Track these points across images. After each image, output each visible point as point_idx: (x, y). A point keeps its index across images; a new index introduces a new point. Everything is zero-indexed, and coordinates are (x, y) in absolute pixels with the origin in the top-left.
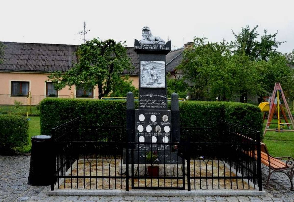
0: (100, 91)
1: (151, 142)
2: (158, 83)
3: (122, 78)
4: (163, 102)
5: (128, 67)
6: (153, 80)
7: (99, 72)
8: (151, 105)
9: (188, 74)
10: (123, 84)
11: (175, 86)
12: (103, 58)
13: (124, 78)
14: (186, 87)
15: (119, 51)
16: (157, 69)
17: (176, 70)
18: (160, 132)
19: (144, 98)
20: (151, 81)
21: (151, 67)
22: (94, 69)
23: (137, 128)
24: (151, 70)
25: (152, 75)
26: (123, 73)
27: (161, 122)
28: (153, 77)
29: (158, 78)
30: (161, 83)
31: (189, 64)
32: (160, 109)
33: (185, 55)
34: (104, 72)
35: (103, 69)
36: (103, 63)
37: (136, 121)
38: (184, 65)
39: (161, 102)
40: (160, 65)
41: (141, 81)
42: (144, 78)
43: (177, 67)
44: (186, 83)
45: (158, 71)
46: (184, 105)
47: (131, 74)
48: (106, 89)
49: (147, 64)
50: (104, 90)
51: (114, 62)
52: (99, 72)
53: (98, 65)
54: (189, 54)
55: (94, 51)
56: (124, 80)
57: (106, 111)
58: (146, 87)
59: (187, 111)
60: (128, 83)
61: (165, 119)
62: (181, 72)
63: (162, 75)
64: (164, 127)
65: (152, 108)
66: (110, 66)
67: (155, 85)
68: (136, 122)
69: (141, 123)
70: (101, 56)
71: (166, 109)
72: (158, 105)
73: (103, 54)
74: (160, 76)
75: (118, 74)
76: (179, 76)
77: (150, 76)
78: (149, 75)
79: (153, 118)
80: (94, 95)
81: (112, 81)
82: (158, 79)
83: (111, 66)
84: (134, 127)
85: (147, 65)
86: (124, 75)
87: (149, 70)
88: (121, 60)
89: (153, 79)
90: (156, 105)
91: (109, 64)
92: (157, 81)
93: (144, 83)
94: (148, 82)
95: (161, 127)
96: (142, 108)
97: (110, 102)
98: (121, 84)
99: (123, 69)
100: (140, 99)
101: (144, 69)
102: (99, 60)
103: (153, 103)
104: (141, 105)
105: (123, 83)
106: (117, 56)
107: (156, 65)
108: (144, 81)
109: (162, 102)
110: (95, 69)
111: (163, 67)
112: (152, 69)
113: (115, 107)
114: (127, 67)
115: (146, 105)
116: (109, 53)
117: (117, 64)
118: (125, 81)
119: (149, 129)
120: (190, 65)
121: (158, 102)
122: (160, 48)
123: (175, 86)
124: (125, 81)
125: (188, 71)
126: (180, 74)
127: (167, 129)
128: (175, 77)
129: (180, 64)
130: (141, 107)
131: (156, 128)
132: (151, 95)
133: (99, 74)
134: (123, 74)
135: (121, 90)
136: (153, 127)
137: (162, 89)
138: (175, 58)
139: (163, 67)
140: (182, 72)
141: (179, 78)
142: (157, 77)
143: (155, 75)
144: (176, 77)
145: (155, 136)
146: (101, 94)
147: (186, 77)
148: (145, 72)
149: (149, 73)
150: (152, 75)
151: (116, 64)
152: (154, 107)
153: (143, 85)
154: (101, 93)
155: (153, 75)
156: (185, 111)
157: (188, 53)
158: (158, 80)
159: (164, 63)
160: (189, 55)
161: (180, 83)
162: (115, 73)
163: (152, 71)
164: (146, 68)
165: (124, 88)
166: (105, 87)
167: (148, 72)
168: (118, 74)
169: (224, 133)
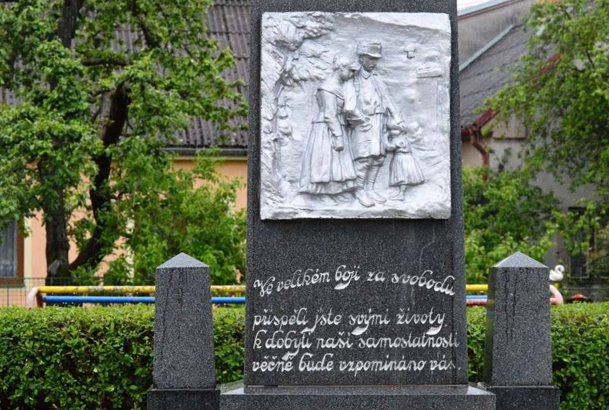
0: (55, 247)
2: (398, 185)
3: (175, 170)
4: (433, 331)
5: (219, 103)
6: (358, 159)
7: (41, 136)
8: (341, 355)
9: (559, 137)
10: (183, 205)
11: (480, 209)
12: (66, 56)
13: (188, 169)
14: (542, 215)
15: (166, 16)
16: (385, 73)
17: (488, 116)
19: (283, 304)
20: (345, 169)
21: (344, 60)
22: (15, 120)
24: (343, 80)
25: (350, 123)
26: (188, 145)
28: (361, 137)
29: (397, 142)
30: (422, 183)
31: (562, 81)
32: (411, 378)
33: (541, 30)
34: (74, 137)
35: (69, 117)
36: (71, 84)
38: (537, 89)
39: (419, 330)
40: (410, 45)
41: (264, 174)
42: (286, 149)
43: (494, 98)
44: (546, 192)
45: (398, 87)
46: (573, 335)
47: (236, 146)
48: (88, 236)
49: (313, 37)
50: (80, 240)
51: (132, 79)
52: (41, 136)
53: (38, 100)
54: (567, 22)
55: (17, 14)
56: (189, 181)
57: (29, 392)
58: (304, 215)
59: (588, 373)
60: (212, 199)
62: (514, 127)
63: (424, 116)
65: (348, 379)
66: (108, 100)
67: (376, 200)
70: (56, 42)
71: (453, 379)
73: (73, 35)
74: (414, 125)
75: (154, 150)
76: (505, 152)
77: (338, 131)
78: (326, 122)
80: (28, 272)
81: (124, 190)
82: (395, 151)
83: (113, 98)
85: (308, 46)
86: (193, 154)
87: (331, 84)
88: (173, 67)
89: (354, 150)
90: (380, 354)
91: (104, 91)
92: (385, 169)
93: (285, 186)
94: (317, 178)
96: (274, 379)
97: (60, 325)
98: (174, 203)
99: (185, 118)
100: (254, 303)
101: (285, 79)
102: (44, 64)
103: (355, 339)
104: (258, 355)
105: (185, 200)
106: (153, 43)
107: (379, 39)
108: (285, 171)
109: (427, 326)
110: (20, 123)
111: (431, 59)
112: (354, 74)
113: (95, 361)
114: (208, 108)
115: (302, 351)
116: (109, 29)
117: (151, 90)
118: (198, 184)
120: (565, 87)
121: (393, 331)
123: (480, 209)
124: (198, 184)
125: (556, 124)
126: (509, 139)
128: (480, 156)
129: (510, 82)
130: (266, 367)
132: (344, 280)
133: (41, 148)
134: (189, 150)
135: (171, 240)
137: (426, 224)
138: (486, 48)
139: (431, 59)
140: (523, 128)
141: (505, 161)
142: (391, 137)
143: (376, 123)
144: (486, 161)
146: (57, 263)
147: (543, 154)
148: (297, 96)
149: (330, 101)
150: (350, 123)
151: (143, 88)
152: (361, 366)
153: (284, 202)
154: (57, 257)
155: (360, 122)
156: (572, 378)
157: (558, 19)
158: (400, 157)
159: (440, 21)
160: (566, 28)
161: (509, 192)
162: (139, 141)
163: (349, 89)
164: (303, 68)
165: (189, 228)
166: (83, 224)
167: (319, 99)
168: (154, 150)
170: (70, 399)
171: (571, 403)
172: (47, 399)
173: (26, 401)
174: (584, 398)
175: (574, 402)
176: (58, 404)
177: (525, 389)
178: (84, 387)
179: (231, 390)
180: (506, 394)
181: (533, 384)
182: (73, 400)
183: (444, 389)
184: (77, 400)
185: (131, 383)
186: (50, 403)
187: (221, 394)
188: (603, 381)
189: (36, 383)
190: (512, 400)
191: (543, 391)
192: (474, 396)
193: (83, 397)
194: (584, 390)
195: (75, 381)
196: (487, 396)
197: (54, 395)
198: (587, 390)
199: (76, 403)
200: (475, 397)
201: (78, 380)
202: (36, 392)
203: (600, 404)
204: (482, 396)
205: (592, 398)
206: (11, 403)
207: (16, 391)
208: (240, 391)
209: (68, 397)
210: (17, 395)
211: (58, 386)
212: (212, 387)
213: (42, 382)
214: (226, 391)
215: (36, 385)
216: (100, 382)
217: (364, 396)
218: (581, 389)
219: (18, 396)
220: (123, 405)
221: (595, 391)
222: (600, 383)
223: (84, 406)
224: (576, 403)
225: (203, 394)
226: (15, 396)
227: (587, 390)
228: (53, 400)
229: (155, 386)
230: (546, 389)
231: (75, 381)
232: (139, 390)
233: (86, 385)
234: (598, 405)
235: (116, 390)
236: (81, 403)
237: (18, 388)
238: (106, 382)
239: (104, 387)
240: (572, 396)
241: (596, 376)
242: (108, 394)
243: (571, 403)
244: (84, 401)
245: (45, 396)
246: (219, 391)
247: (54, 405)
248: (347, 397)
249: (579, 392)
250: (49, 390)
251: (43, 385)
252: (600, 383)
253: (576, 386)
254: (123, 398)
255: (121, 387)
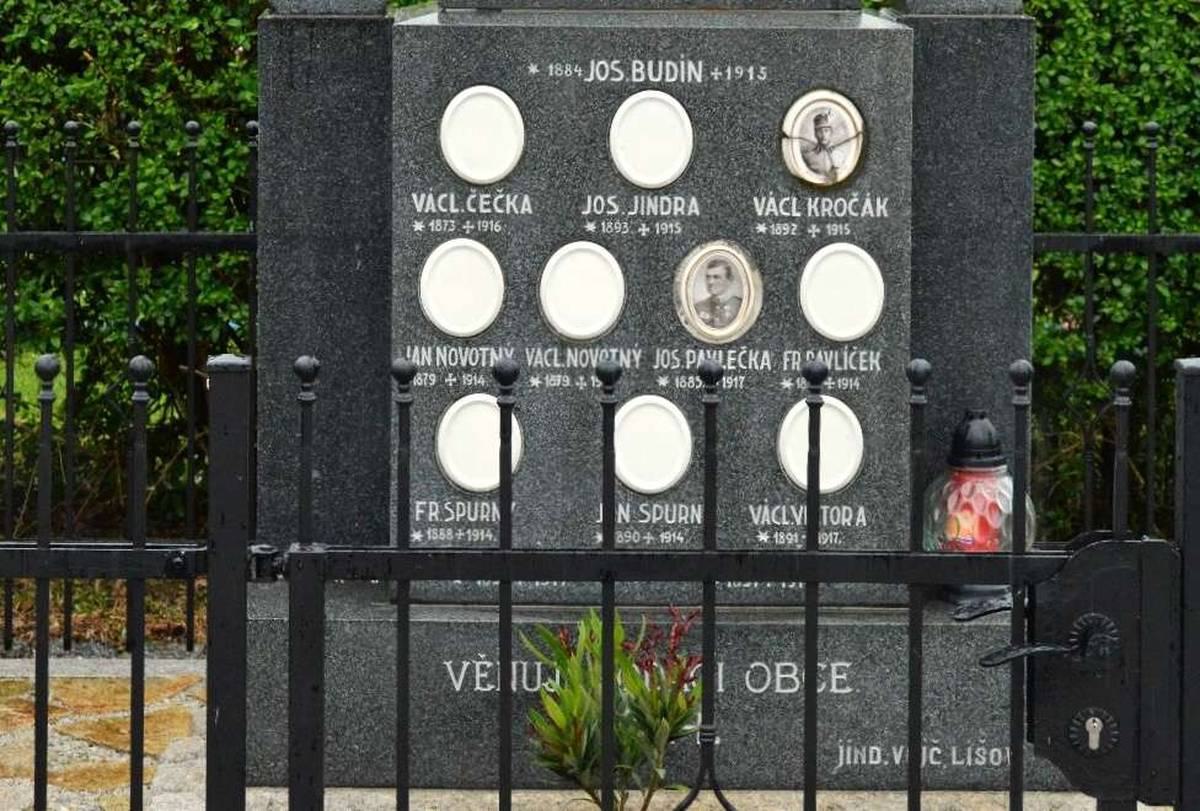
23: (413, 279)
27: (754, 184)
37: (397, 188)
57: (39, 29)
61: (820, 146)
64: (800, 266)
68: (397, 203)
69: (468, 208)
79: (652, 139)
84: (372, 281)
95: (758, 259)
119: (584, 290)
127: (845, 293)
131: (691, 282)
136: (649, 267)
145: (669, 393)
169: (157, 358)
170: (116, 43)
171: (1060, 58)
172: (73, 43)
173: (35, 46)
174: (1085, 49)
175: (1065, 57)
176: (94, 53)
177: (970, 19)
178: (142, 21)
179: (414, 16)
180: (934, 29)
181: (985, 11)
182: (122, 46)
183: (817, 18)
184: (128, 44)
185: (229, 14)
186: (79, 50)
187: (395, 24)
188: (1122, 17)
189: (53, 12)
190: (945, 40)
191: (1004, 24)
192: (872, 31)
193: (140, 40)
194: (1085, 34)
195: (126, 9)
196: (897, 32)
197: (86, 36)
198: (1091, 35)
199: (127, 51)
200: (870, 35)
201: (131, 7)
202: (53, 30)
203: (1116, 60)
204: (886, 31)
205: (1100, 49)
206: (8, 49)
207: (17, 27)
208: (431, 19)
209: (113, 38)
210: (18, 34)
211: (93, 18)
212: (379, 12)
213: (64, 11)
214: (404, 19)
215: (54, 16)
216: (173, 12)
217: (663, 30)
218: (1080, 31)
219: (20, 35)
220: (214, 54)
221: (1107, 36)
222: (1115, 21)
223: (142, 56)
224: (1069, 59)
225: (363, 25)
226: (14, 37)
227: (1091, 35)
228: (84, 45)
229: (273, 10)
230: (1010, 21)
231: (126, 9)
232: (243, 27)
233: (145, 17)
234: (1112, 62)
235: (201, 28)
236: (137, 50)
237: (19, 22)
238: (182, 12)
239: (180, 22)
240: (1062, 45)
241: (1109, 8)
242: (186, 35)
243: (1060, 58)
244: (142, 46)
245: (70, 38)
246: (393, 20)
247: (86, 54)
248: (633, 30)
249: (1075, 39)
250: (78, 27)
251: (66, 16)
252: (1115, 21)
253: (1071, 28)
254: (214, 43)
255: (212, 22)
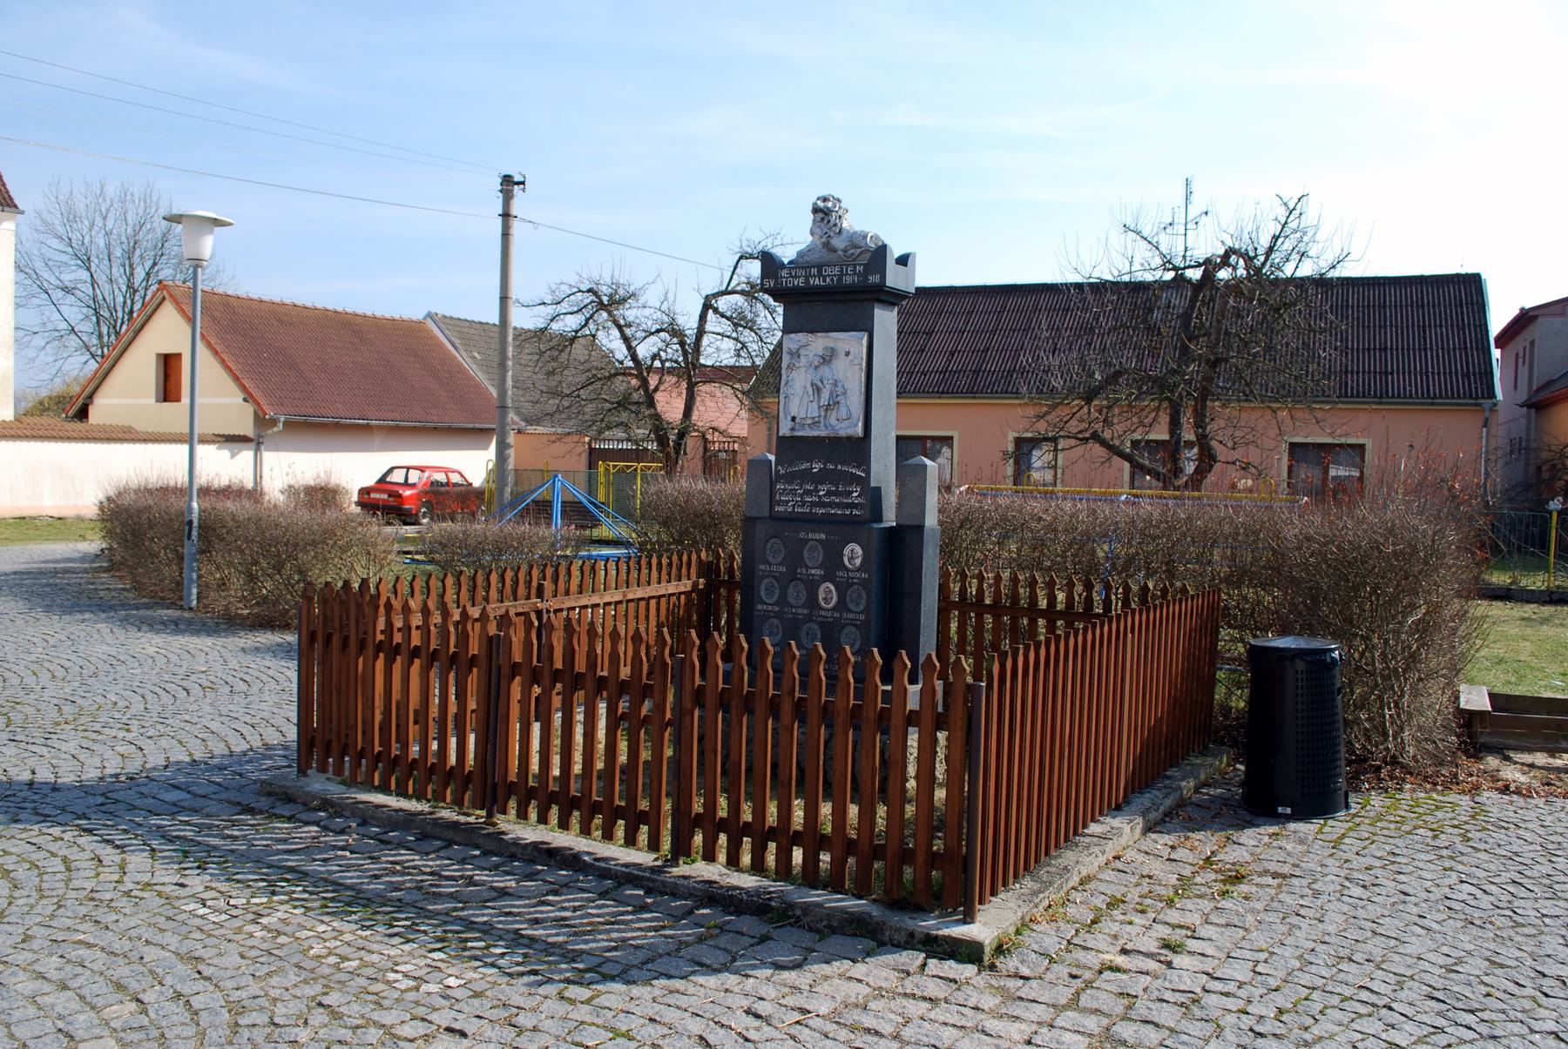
1: (496, 329)
8: (813, 504)
18: (834, 609)
72: (838, 505)
90: (831, 505)
121: (836, 494)
122: (848, 280)
132: (817, 467)
